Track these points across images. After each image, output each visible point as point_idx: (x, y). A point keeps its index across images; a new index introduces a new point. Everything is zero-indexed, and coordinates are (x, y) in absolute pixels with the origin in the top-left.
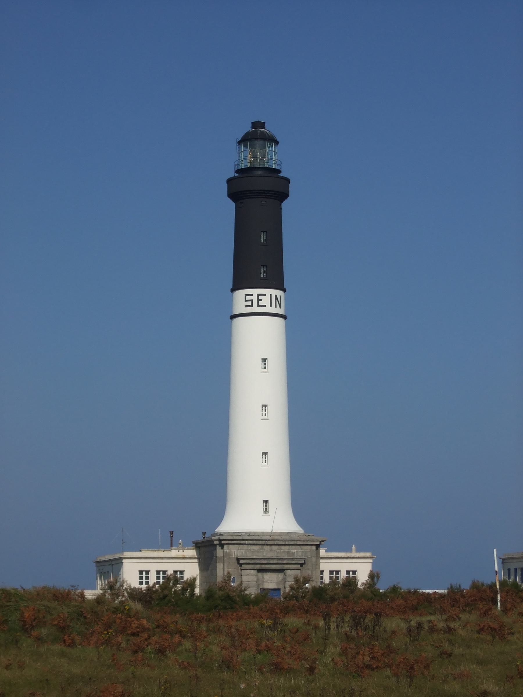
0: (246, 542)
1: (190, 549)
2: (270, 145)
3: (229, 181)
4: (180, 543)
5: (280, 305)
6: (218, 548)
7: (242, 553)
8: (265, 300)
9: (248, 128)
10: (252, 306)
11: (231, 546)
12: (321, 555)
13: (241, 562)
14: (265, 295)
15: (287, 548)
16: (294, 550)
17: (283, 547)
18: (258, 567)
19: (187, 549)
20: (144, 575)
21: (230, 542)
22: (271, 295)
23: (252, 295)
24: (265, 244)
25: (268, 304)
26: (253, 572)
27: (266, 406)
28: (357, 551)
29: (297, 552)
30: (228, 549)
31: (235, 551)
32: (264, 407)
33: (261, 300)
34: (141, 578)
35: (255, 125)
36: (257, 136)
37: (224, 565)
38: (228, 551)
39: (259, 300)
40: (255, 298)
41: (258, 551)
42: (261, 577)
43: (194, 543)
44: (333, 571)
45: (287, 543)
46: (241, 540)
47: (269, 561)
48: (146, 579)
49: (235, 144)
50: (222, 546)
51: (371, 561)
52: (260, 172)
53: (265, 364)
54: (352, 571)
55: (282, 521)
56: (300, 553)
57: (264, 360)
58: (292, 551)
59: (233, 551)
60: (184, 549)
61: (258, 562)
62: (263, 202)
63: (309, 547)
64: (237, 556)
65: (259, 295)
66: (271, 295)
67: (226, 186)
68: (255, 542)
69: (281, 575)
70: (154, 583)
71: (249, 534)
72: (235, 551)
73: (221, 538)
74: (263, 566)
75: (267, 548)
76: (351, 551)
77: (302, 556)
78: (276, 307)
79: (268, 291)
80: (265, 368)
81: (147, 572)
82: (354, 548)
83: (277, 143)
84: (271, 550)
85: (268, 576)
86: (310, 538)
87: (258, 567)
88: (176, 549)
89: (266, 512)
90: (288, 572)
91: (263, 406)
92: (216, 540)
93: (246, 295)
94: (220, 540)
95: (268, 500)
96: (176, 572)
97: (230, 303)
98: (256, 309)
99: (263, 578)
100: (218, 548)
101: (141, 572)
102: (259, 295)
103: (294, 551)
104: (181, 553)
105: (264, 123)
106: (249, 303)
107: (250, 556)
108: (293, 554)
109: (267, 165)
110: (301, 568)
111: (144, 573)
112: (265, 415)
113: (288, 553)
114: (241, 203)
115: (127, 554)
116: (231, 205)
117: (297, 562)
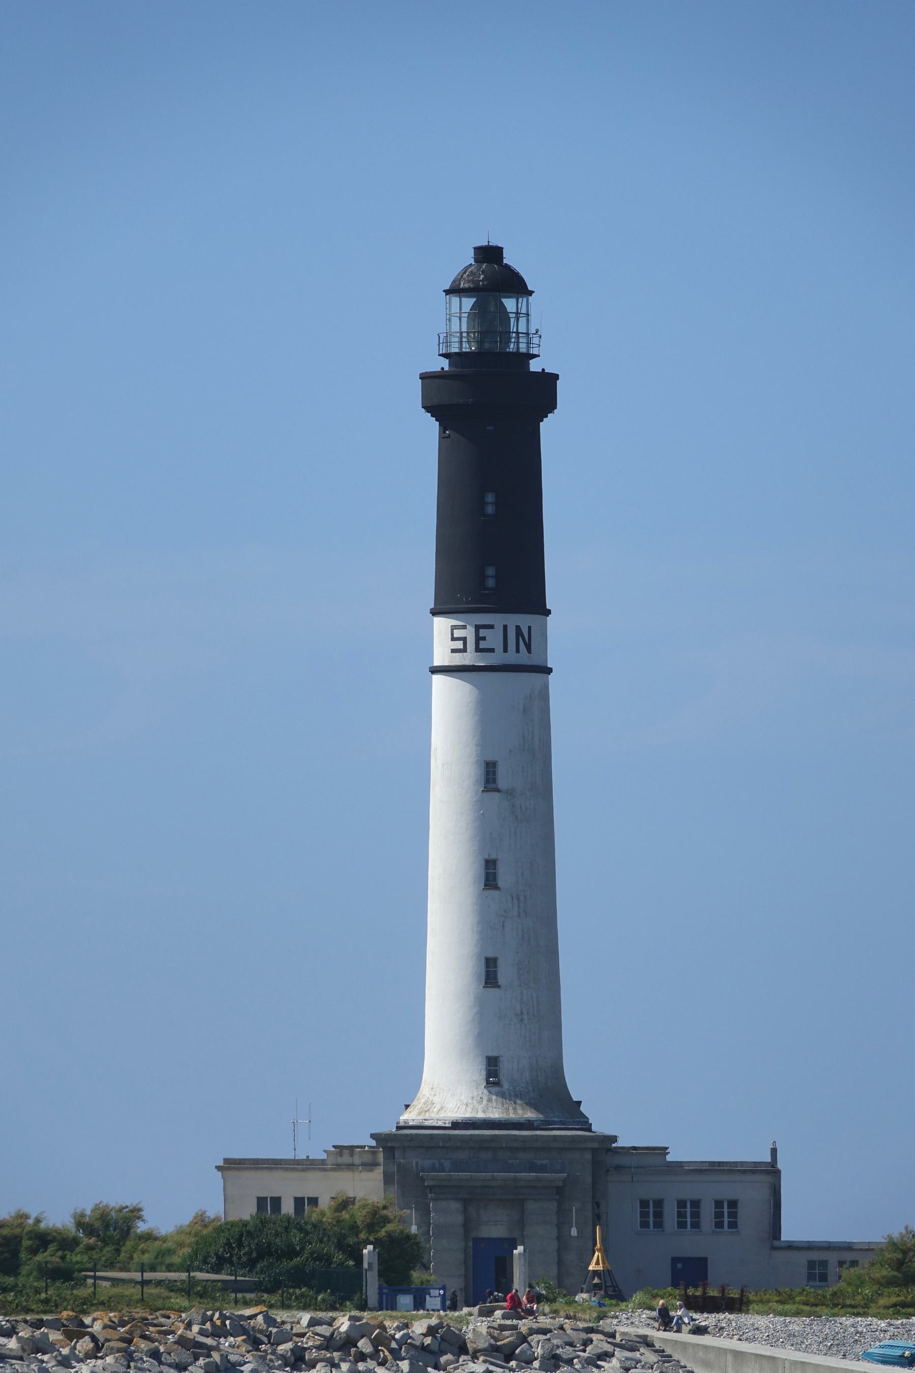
10: (464, 650)
14: (491, 627)
22: (505, 627)
25: (499, 647)
30: (404, 1158)
33: (484, 639)
34: (645, 1215)
36: (493, 280)
39: (478, 639)
66: (505, 627)
70: (112, 1231)
78: (518, 651)
81: (696, 1204)
101: (644, 1204)
105: (556, 377)
106: (459, 645)
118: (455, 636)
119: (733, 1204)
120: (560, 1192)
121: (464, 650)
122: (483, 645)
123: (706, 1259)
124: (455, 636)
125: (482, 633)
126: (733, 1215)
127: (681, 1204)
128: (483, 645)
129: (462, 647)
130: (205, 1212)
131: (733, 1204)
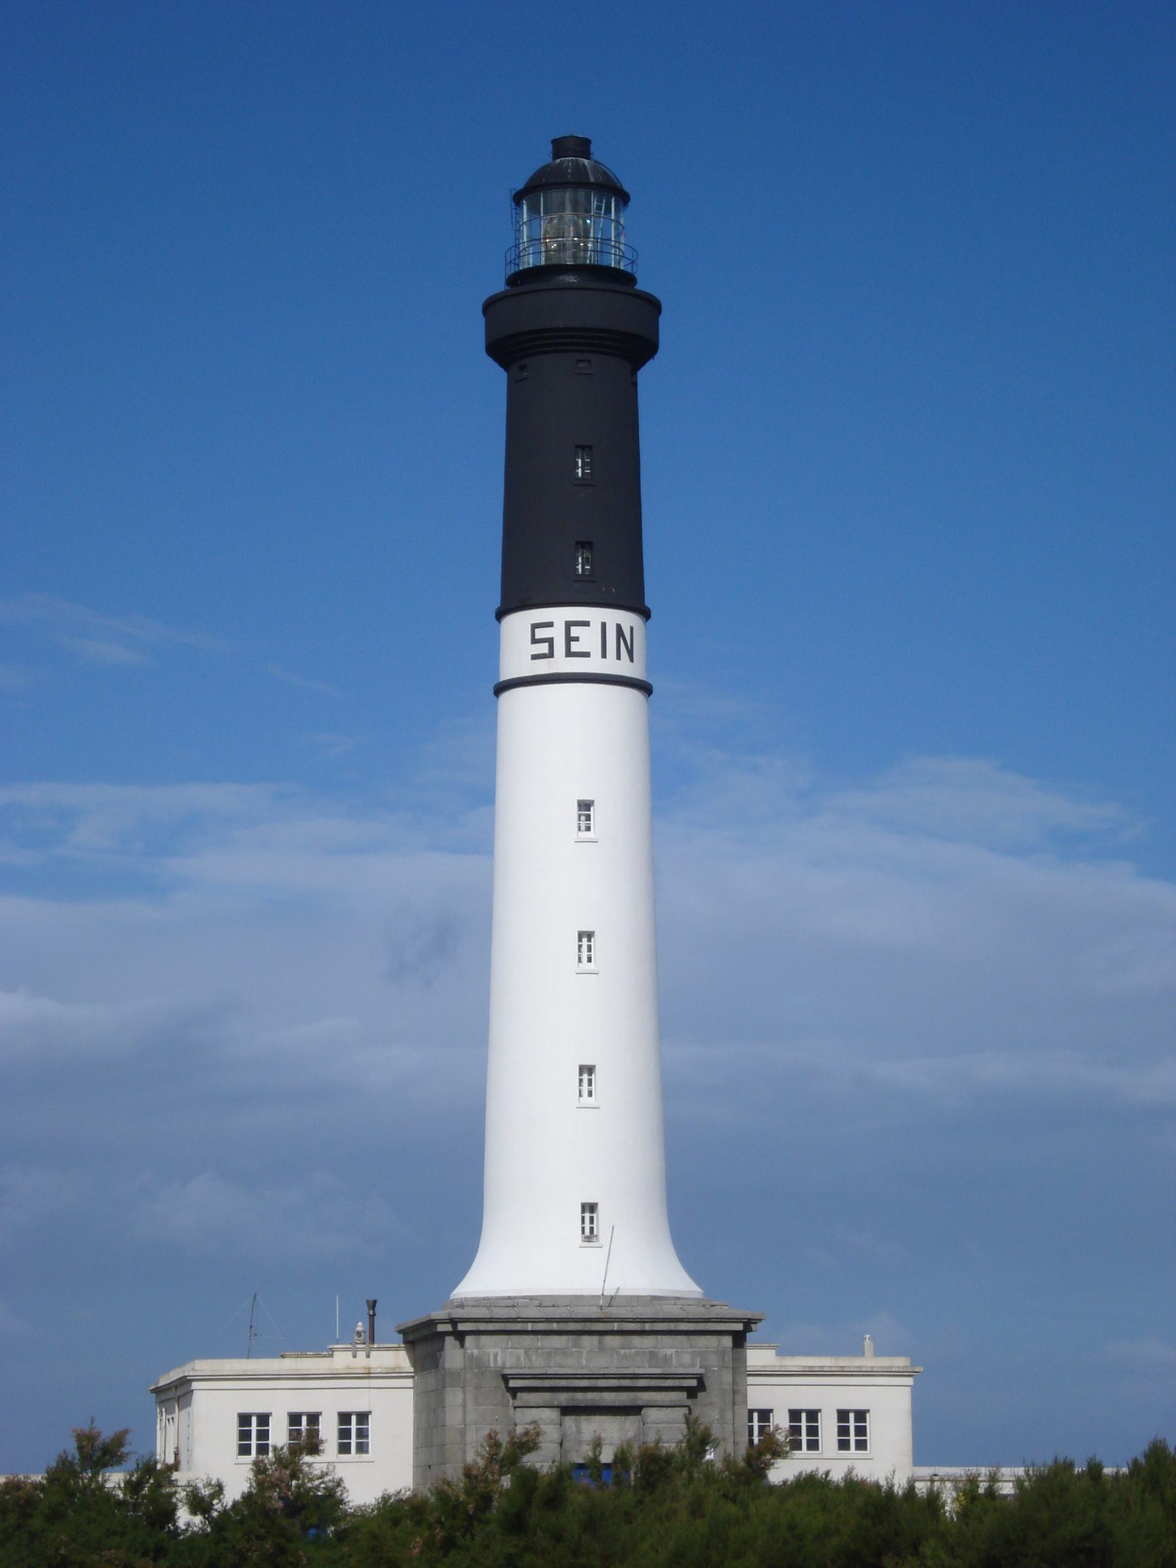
0: (530, 1327)
1: (388, 1349)
2: (600, 201)
3: (490, 306)
4: (359, 1334)
5: (630, 653)
6: (450, 1341)
7: (518, 1358)
8: (588, 639)
9: (543, 157)
10: (551, 655)
11: (484, 1339)
12: (749, 1363)
13: (512, 1384)
14: (586, 624)
15: (648, 1342)
16: (668, 1347)
17: (637, 1340)
18: (563, 1398)
19: (379, 1349)
20: (254, 1428)
21: (482, 1327)
22: (604, 625)
24: (583, 483)
25: (596, 650)
27: (590, 935)
28: (878, 1353)
29: (681, 1357)
30: (478, 1346)
31: (501, 1354)
32: (585, 940)
33: (577, 639)
35: (560, 147)
36: (570, 175)
37: (464, 1393)
38: (476, 1352)
39: (569, 639)
40: (557, 634)
41: (563, 1352)
42: (574, 1428)
43: (404, 1332)
45: (648, 1327)
47: (594, 1382)
48: (258, 1438)
49: (508, 202)
50: (460, 1336)
51: (910, 1381)
52: (571, 279)
53: (588, 818)
55: (637, 1265)
56: (687, 1359)
57: (585, 806)
59: (492, 1351)
60: (371, 1350)
61: (563, 1383)
63: (712, 1340)
64: (504, 1367)
65: (569, 625)
66: (604, 625)
67: (481, 322)
68: (555, 1326)
71: (539, 1301)
72: (501, 1354)
73: (458, 1313)
74: (579, 1396)
75: (588, 1342)
77: (693, 1365)
78: (619, 657)
80: (588, 829)
81: (813, 1415)
82: (868, 1344)
83: (624, 199)
84: (601, 1348)
85: (591, 1426)
86: (715, 1313)
87: (563, 1398)
88: (346, 1350)
89: (590, 1236)
90: (651, 1414)
91: (581, 935)
92: (443, 1322)
93: (535, 626)
94: (453, 1322)
95: (596, 1204)
97: (492, 651)
98: (561, 664)
99: (579, 1432)
100: (450, 1341)
101: (244, 1419)
102: (569, 625)
103: (669, 1352)
104: (361, 1361)
106: (544, 648)
107: (538, 1364)
108: (667, 1360)
109: (590, 259)
110: (689, 1402)
111: (254, 1420)
112: (589, 960)
113: (653, 1355)
114: (522, 368)
115: (203, 1366)
116: (496, 377)
117: (676, 1383)
118: (547, 645)
119: (861, 1415)
121: (551, 655)
122: (575, 647)
124: (547, 645)
125: (575, 631)
127: (843, 1415)
128: (575, 647)
129: (537, 630)
131: (861, 1415)
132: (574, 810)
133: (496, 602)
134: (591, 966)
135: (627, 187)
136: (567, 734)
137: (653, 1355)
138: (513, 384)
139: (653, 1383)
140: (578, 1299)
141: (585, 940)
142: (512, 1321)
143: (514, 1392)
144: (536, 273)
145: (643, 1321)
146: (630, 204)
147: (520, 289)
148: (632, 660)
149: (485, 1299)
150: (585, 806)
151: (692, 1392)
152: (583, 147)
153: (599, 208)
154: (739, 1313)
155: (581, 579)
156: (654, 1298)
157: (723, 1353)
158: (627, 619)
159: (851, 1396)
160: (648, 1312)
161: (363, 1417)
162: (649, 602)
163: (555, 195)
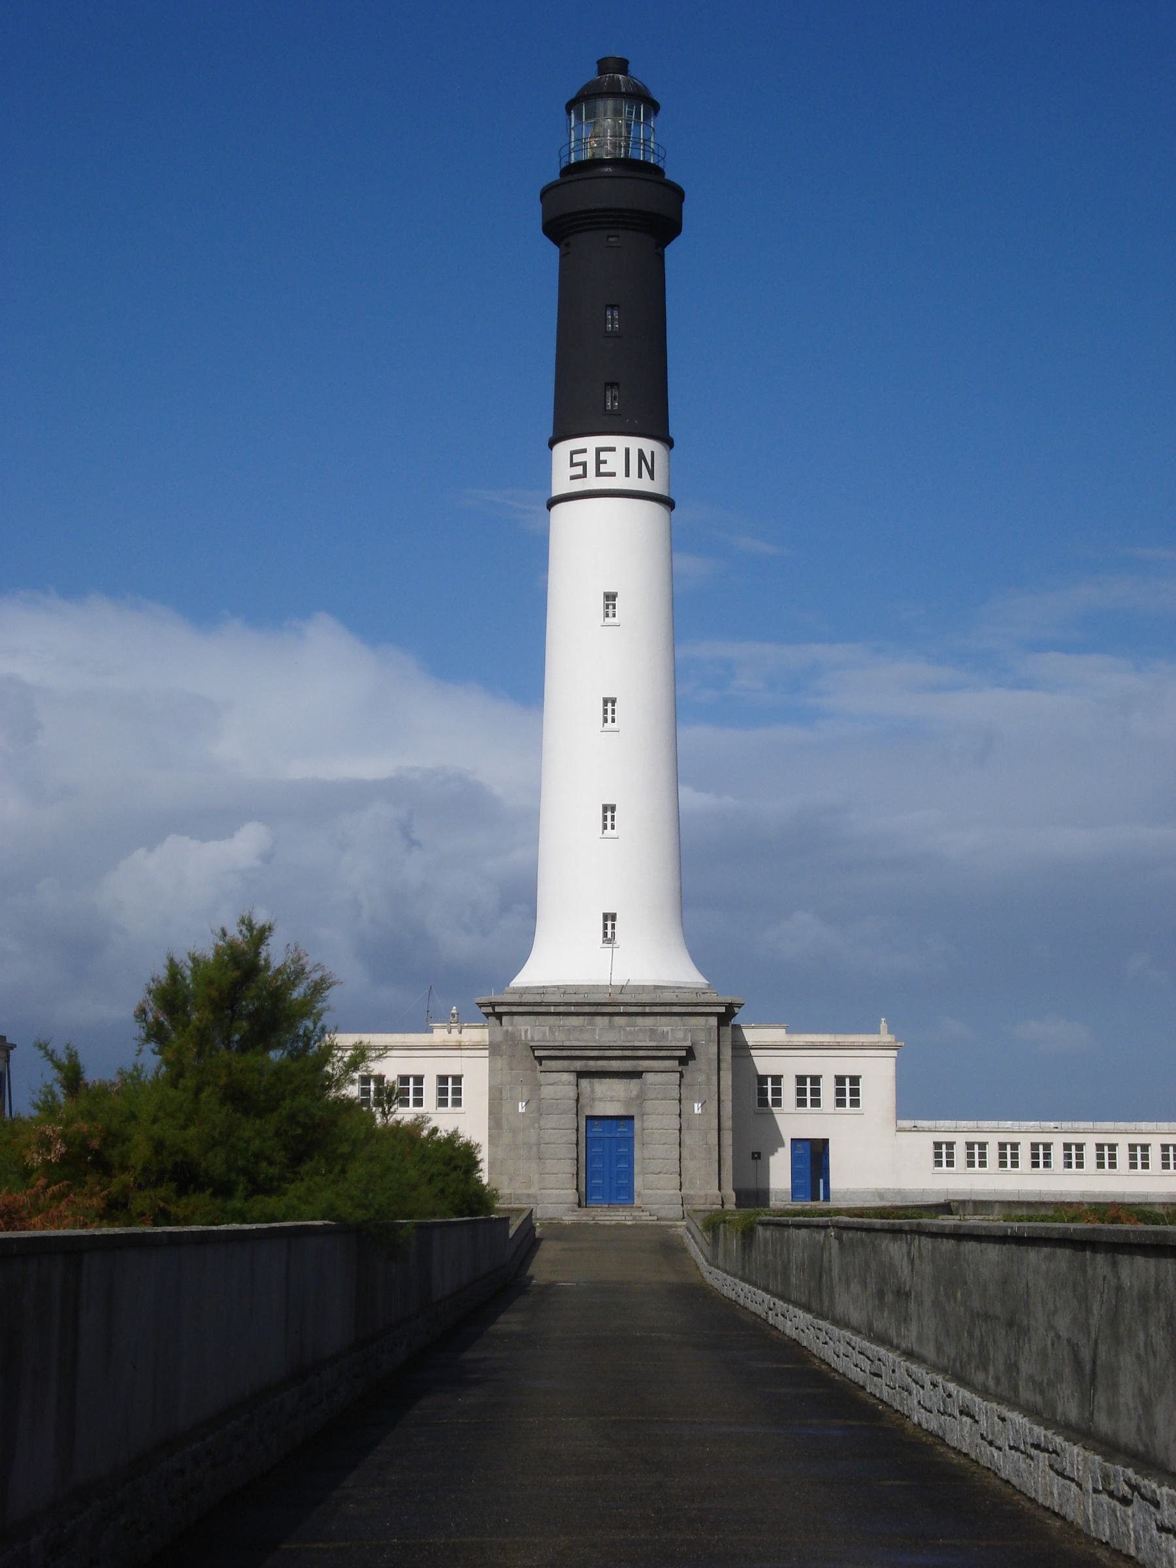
0: (552, 1009)
1: (476, 1027)
2: (631, 107)
3: (546, 193)
4: (453, 1015)
7: (544, 1034)
8: (614, 462)
9: (590, 74)
10: (584, 475)
13: (537, 1053)
14: (613, 449)
15: (649, 1021)
18: (578, 1065)
21: (515, 1009)
22: (627, 450)
23: (584, 451)
25: (621, 471)
26: (567, 1077)
30: (512, 1024)
32: (609, 705)
33: (605, 462)
35: (604, 66)
36: (613, 84)
38: (510, 1028)
39: (599, 462)
40: (590, 458)
41: (580, 1029)
44: (767, 1076)
45: (647, 1009)
46: (539, 1004)
47: (603, 1052)
48: (453, 1094)
51: (894, 1053)
52: (608, 169)
54: (773, 1077)
55: (651, 960)
56: (680, 1035)
57: (610, 597)
58: (660, 1029)
59: (523, 1028)
61: (578, 1053)
62: (611, 239)
63: (702, 1020)
64: (533, 1040)
65: (599, 451)
66: (627, 450)
67: (538, 207)
68: (573, 1009)
69: (633, 1085)
71: (564, 989)
74: (592, 1063)
76: (877, 1031)
77: (685, 1040)
78: (640, 476)
79: (620, 442)
81: (816, 1080)
82: (883, 1025)
83: (653, 107)
84: (611, 1026)
85: (603, 1087)
87: (578, 1065)
88: (443, 1027)
89: (608, 938)
90: (650, 1078)
93: (573, 453)
96: (404, 1079)
99: (593, 1091)
102: (599, 451)
103: (665, 1029)
104: (455, 1037)
106: (579, 470)
107: (560, 1039)
108: (664, 1035)
113: (653, 1031)
116: (554, 251)
118: (574, 461)
119: (855, 1080)
120: (688, 1056)
123: (825, 1142)
124: (574, 461)
125: (603, 456)
126: (855, 1092)
127: (840, 1080)
130: (259, 936)
131: (855, 1080)
132: (600, 601)
133: (549, 433)
134: (615, 726)
135: (656, 95)
136: (602, 544)
137: (653, 1031)
138: (562, 256)
139: (650, 1053)
140: (595, 988)
141: (609, 705)
142: (539, 1006)
143: (540, 1059)
144: (581, 166)
145: (644, 1005)
146: (661, 112)
147: (571, 178)
148: (652, 478)
149: (539, 987)
150: (610, 597)
151: (683, 1061)
152: (622, 65)
153: (630, 113)
154: (722, 999)
155: (612, 413)
156: (656, 987)
157: (709, 1030)
158: (648, 445)
159: (847, 1065)
160: (646, 998)
161: (457, 1079)
162: (672, 433)
163: (600, 104)
